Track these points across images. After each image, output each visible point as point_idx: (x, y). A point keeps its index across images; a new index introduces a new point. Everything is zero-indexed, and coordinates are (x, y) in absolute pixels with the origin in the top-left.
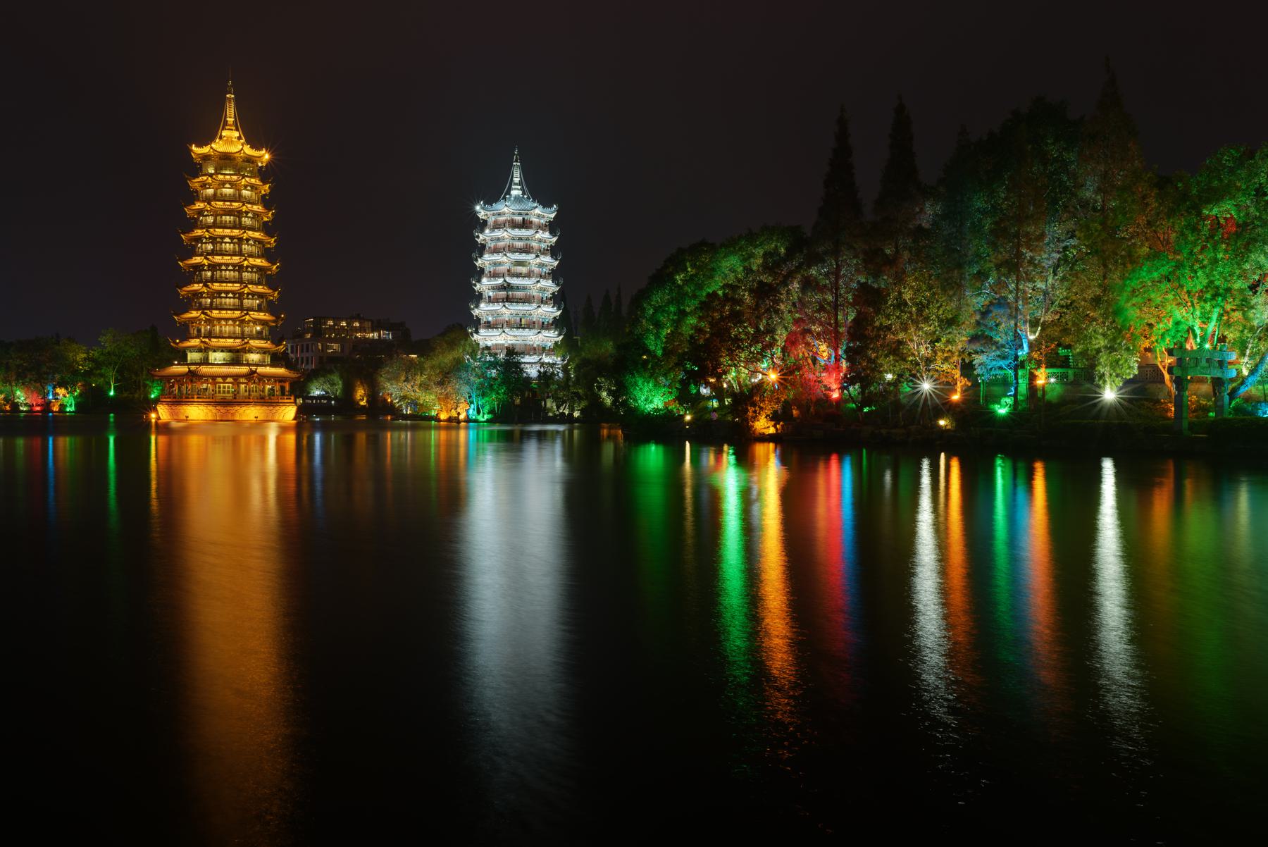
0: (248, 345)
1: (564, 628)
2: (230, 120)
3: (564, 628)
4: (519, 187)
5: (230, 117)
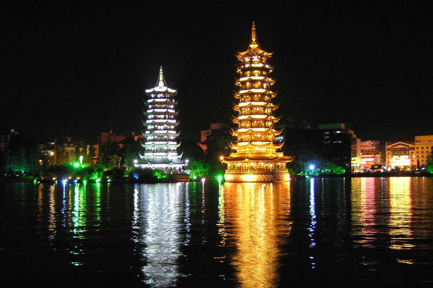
2: (254, 40)
5: (254, 38)
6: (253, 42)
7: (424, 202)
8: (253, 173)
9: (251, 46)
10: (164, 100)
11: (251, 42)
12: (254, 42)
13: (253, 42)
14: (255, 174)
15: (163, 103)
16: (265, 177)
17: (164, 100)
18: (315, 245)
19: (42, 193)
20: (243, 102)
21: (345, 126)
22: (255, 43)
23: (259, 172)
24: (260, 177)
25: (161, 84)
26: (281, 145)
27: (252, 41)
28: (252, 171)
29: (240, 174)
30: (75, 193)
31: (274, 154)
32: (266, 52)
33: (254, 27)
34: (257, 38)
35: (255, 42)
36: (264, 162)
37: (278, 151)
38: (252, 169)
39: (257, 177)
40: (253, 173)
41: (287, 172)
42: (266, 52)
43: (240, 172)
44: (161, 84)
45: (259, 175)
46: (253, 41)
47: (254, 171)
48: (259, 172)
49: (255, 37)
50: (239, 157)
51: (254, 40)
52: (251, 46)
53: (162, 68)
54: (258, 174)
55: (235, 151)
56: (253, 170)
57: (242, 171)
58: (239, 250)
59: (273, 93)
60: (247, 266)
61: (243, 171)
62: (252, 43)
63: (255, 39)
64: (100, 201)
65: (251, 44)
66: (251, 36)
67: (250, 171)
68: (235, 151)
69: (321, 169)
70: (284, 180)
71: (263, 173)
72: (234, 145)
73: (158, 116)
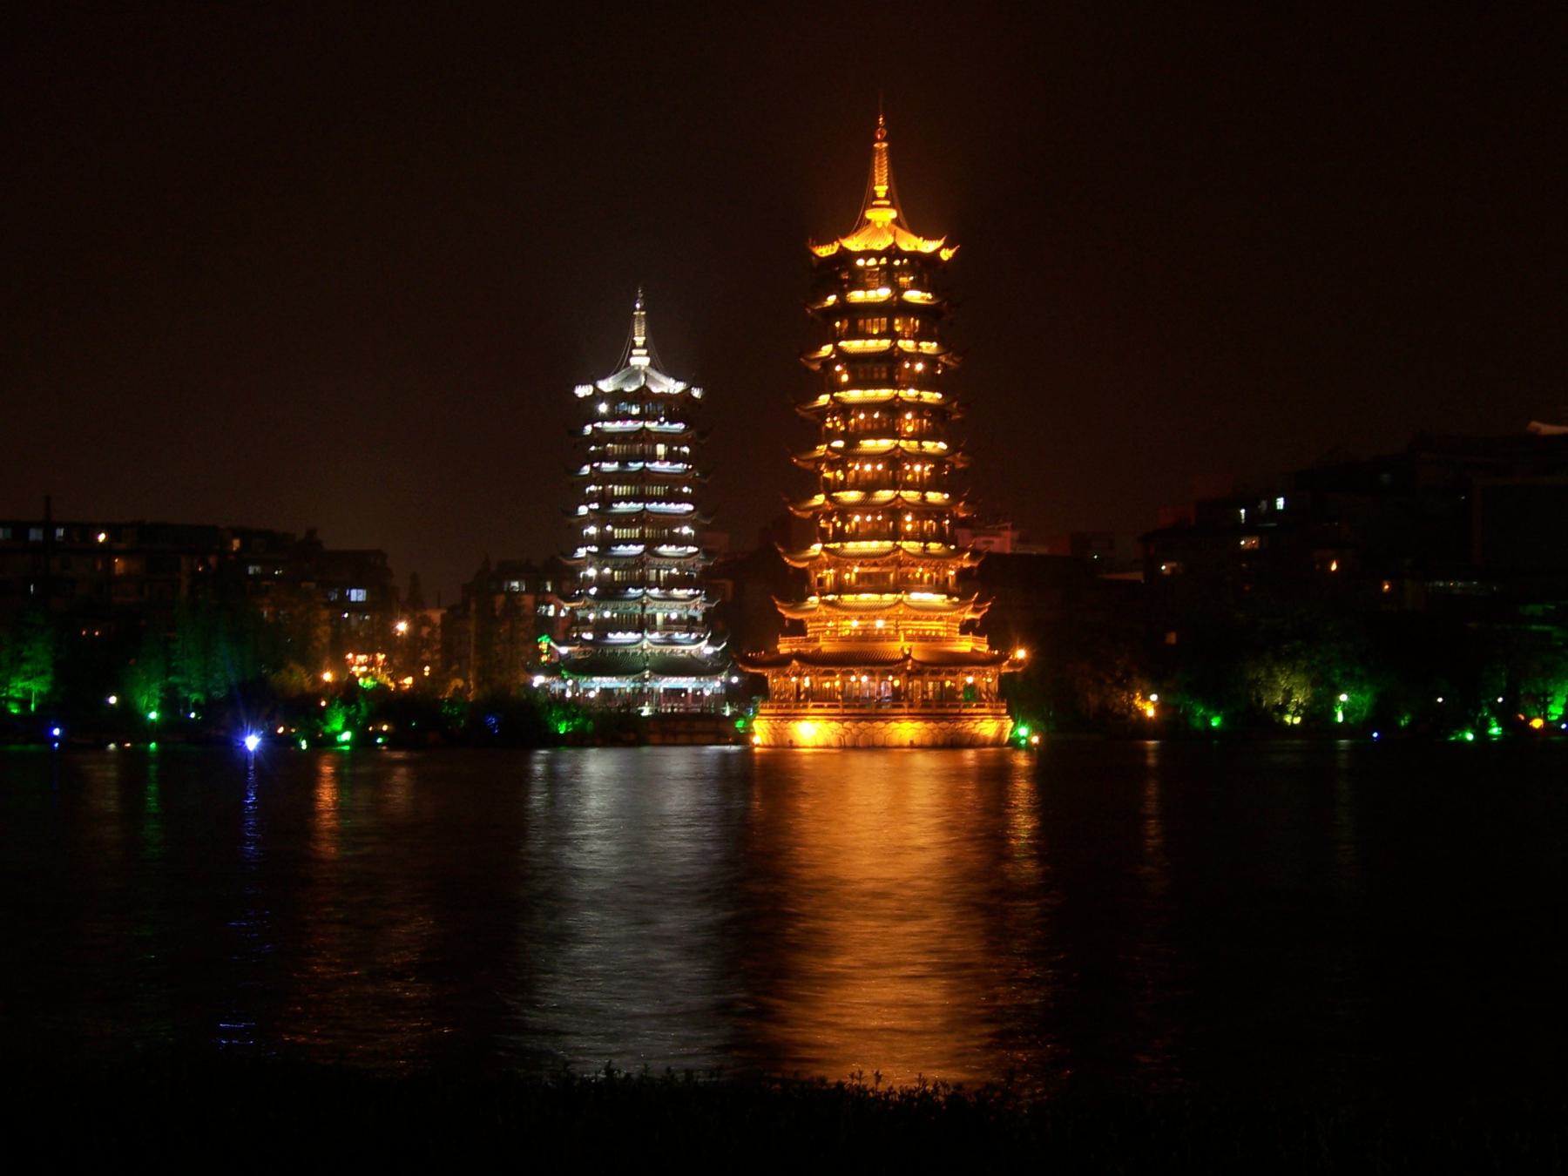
2: (881, 190)
5: (640, 336)
8: (828, 715)
10: (636, 426)
11: (870, 200)
14: (817, 720)
15: (632, 438)
16: (854, 731)
17: (636, 426)
19: (710, 796)
21: (150, 712)
22: (887, 203)
23: (846, 711)
24: (850, 730)
25: (882, 216)
28: (822, 707)
29: (870, 717)
33: (885, 140)
35: (886, 198)
36: (871, 674)
37: (967, 628)
39: (841, 731)
40: (828, 715)
43: (787, 711)
44: (882, 216)
45: (847, 724)
47: (829, 707)
48: (846, 711)
49: (643, 333)
51: (881, 190)
53: (642, 298)
54: (843, 718)
56: (826, 704)
57: (793, 706)
61: (797, 707)
63: (644, 338)
64: (574, 820)
67: (814, 707)
68: (798, 628)
69: (573, 722)
71: (850, 715)
72: (785, 605)
73: (616, 488)
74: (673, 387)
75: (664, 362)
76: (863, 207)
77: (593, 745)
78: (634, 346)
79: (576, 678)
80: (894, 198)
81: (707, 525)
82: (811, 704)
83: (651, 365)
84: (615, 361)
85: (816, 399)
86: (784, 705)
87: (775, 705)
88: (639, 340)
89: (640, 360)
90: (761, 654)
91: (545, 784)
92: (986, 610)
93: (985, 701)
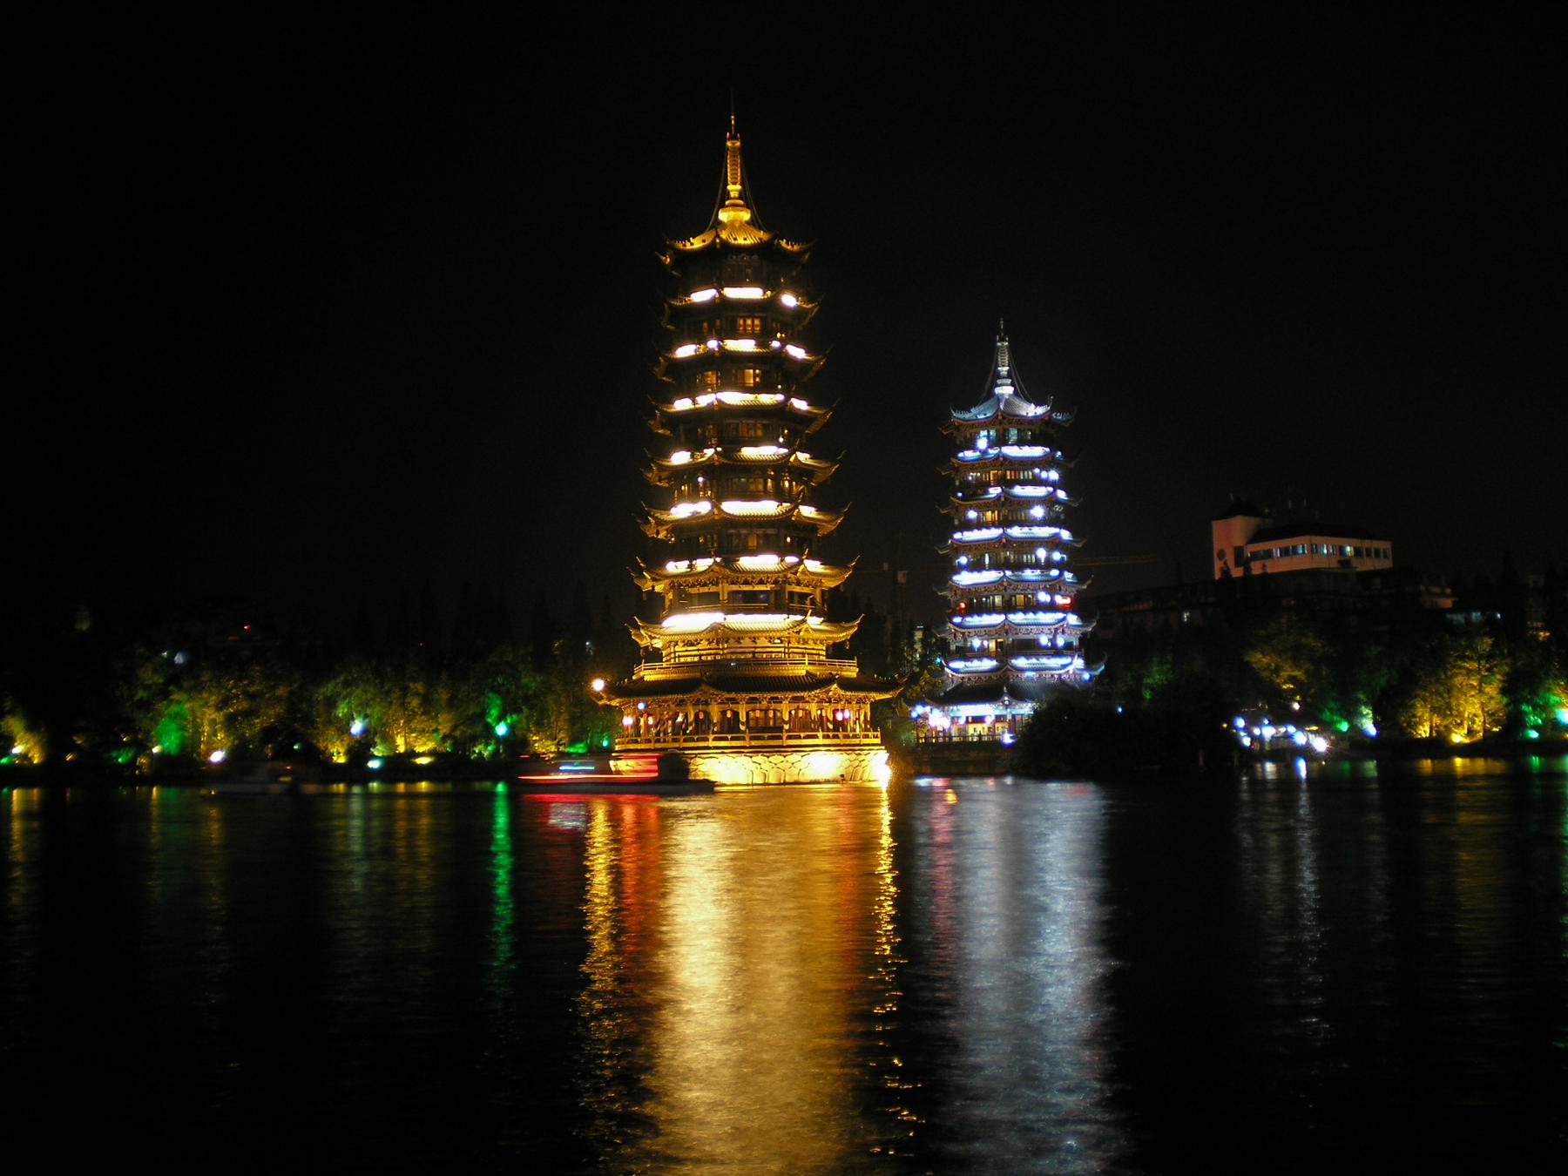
0: (805, 626)
1: (971, 924)
2: (734, 189)
3: (971, 924)
4: (1009, 381)
5: (734, 184)
6: (729, 198)
7: (354, 924)
9: (724, 216)
11: (722, 200)
12: (735, 198)
13: (729, 198)
18: (656, 774)
20: (747, 632)
23: (753, 743)
26: (853, 627)
27: (726, 195)
28: (725, 739)
30: (665, 880)
31: (821, 663)
32: (822, 619)
34: (747, 184)
38: (725, 730)
41: (878, 741)
42: (822, 619)
46: (732, 194)
48: (753, 743)
50: (666, 680)
51: (734, 189)
52: (724, 216)
55: (654, 656)
56: (766, 735)
58: (915, 874)
59: (828, 571)
60: (812, 944)
62: (727, 203)
65: (722, 206)
66: (724, 170)
67: (715, 739)
70: (840, 976)
74: (1031, 410)
75: (1028, 392)
76: (717, 206)
77: (422, 793)
78: (998, 376)
79: (376, 711)
80: (747, 199)
81: (1079, 548)
82: (711, 737)
83: (1015, 393)
84: (983, 393)
85: (671, 402)
86: (696, 737)
87: (831, 734)
88: (1004, 370)
89: (1006, 390)
90: (624, 682)
91: (812, 822)
92: (856, 629)
93: (744, 732)
